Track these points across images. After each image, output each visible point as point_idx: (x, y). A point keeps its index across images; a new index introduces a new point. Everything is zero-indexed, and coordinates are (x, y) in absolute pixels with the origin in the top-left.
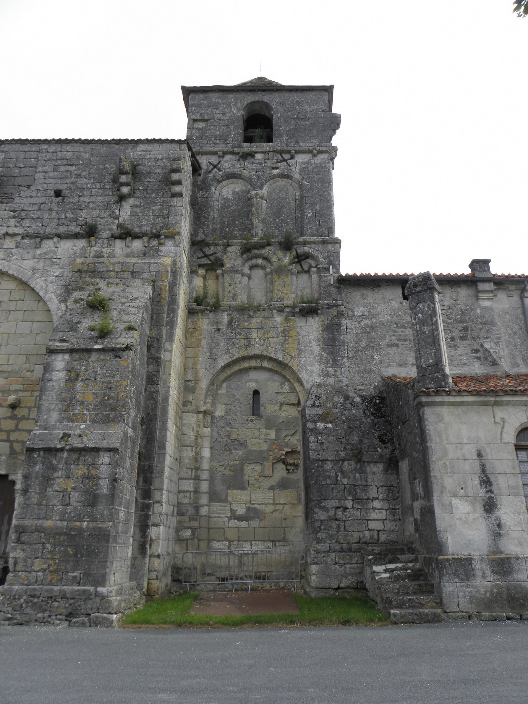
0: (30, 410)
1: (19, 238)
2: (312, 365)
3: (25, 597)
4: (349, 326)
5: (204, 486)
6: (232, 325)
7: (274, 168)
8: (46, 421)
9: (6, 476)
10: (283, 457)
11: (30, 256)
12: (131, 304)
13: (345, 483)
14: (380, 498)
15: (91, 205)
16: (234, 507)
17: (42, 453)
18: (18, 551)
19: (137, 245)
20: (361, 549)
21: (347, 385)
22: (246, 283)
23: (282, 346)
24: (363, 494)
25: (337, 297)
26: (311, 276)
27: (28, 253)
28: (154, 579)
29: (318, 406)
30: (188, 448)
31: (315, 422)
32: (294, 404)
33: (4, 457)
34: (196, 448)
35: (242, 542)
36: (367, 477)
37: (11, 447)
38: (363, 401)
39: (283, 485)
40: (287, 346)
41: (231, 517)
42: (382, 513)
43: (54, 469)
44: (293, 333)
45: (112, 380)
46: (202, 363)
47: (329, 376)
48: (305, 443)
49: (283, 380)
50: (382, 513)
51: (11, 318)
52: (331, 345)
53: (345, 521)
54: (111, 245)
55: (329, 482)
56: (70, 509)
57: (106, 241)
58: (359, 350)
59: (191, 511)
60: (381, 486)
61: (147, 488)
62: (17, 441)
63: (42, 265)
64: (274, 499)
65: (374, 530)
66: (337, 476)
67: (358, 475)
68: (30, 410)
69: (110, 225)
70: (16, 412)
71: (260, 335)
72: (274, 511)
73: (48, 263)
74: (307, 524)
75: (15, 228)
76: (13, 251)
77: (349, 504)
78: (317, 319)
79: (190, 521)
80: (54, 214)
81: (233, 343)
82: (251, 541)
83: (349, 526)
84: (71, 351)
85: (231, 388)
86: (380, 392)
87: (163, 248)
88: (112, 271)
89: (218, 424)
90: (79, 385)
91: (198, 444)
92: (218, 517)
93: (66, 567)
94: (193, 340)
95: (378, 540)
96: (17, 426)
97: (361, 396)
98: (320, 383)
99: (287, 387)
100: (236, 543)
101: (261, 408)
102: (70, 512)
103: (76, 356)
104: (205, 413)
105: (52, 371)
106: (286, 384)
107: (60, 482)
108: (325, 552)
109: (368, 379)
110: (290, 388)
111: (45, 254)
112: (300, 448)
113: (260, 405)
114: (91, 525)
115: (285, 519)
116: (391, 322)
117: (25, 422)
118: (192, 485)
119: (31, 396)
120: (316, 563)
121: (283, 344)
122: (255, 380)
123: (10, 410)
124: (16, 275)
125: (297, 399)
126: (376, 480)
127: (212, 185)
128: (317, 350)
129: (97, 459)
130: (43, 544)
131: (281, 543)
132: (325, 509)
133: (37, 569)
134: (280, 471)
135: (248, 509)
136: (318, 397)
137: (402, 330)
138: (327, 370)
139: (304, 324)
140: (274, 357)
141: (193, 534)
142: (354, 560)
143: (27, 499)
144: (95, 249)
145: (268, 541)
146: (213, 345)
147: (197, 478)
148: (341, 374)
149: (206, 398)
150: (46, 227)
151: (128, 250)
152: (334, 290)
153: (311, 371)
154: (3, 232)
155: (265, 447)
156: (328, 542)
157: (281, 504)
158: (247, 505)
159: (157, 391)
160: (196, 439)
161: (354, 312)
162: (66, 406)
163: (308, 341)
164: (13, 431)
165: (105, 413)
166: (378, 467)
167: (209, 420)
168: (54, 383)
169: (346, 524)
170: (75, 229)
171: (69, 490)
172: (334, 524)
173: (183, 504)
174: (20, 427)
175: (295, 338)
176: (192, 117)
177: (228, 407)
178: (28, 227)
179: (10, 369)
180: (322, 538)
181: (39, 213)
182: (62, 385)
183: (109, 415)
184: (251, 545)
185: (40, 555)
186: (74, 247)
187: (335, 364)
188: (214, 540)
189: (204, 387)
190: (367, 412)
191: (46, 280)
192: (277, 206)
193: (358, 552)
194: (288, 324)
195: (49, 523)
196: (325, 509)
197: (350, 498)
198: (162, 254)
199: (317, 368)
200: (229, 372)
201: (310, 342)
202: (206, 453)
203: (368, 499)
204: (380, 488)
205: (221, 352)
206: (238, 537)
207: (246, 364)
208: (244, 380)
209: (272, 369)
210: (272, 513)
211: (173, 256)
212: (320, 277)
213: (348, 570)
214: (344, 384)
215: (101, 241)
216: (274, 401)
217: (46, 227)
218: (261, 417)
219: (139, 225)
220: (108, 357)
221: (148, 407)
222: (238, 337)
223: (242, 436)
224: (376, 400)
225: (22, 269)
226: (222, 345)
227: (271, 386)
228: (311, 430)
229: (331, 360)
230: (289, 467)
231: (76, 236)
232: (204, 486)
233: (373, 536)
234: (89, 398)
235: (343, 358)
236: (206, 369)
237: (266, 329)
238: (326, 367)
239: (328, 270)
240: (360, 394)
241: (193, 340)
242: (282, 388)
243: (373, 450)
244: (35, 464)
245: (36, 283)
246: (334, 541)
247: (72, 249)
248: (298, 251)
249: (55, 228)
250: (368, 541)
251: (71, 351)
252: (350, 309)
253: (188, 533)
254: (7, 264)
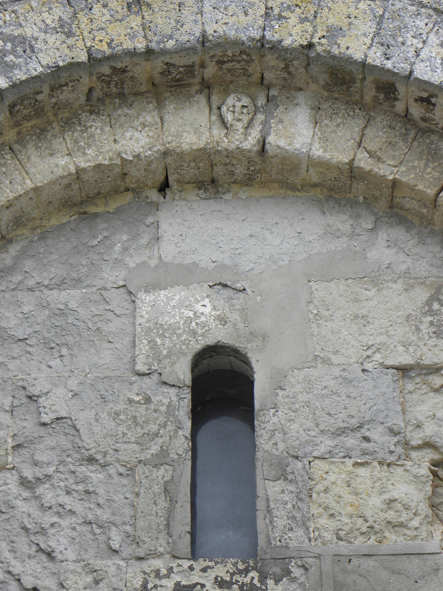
101: (271, 489)
113: (262, 470)
140: (375, 57)
208: (111, 276)
209: (353, 172)
216: (377, 434)
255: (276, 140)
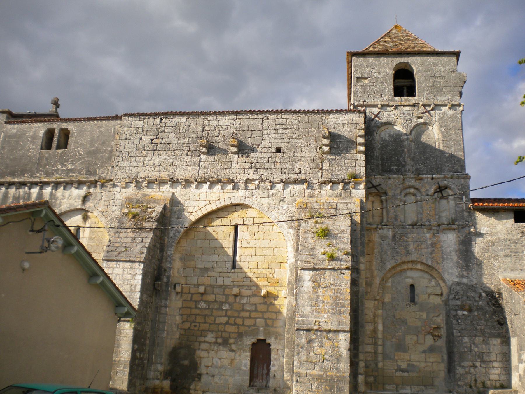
2: (452, 269)
5: (380, 349)
7: (419, 118)
10: (432, 331)
15: (303, 159)
16: (399, 363)
21: (476, 284)
26: (448, 202)
31: (456, 310)
32: (438, 295)
37: (265, 322)
38: (487, 295)
39: (432, 350)
40: (434, 255)
52: (465, 255)
55: (466, 350)
59: (373, 365)
64: (426, 359)
66: (471, 346)
67: (484, 346)
71: (415, 246)
80: (278, 166)
81: (397, 252)
90: (321, 290)
96: (268, 309)
99: (433, 283)
106: (433, 280)
110: (436, 284)
115: (433, 372)
116: (507, 239)
121: (431, 253)
127: (374, 131)
128: (455, 258)
132: (463, 367)
134: (429, 340)
136: (457, 293)
137: (514, 244)
141: (375, 380)
147: (375, 344)
148: (472, 276)
149: (379, 290)
153: (452, 273)
155: (419, 324)
164: (266, 312)
166: (497, 341)
175: (440, 249)
176: (356, 76)
179: (259, 272)
181: (268, 164)
189: (378, 282)
190: (490, 303)
191: (278, 213)
192: (422, 147)
196: (463, 367)
197: (479, 360)
199: (455, 271)
200: (394, 272)
201: (451, 253)
202: (380, 327)
230: (435, 338)
235: (473, 264)
238: (462, 271)
242: (430, 283)
244: (302, 338)
251: (314, 269)
253: (371, 379)
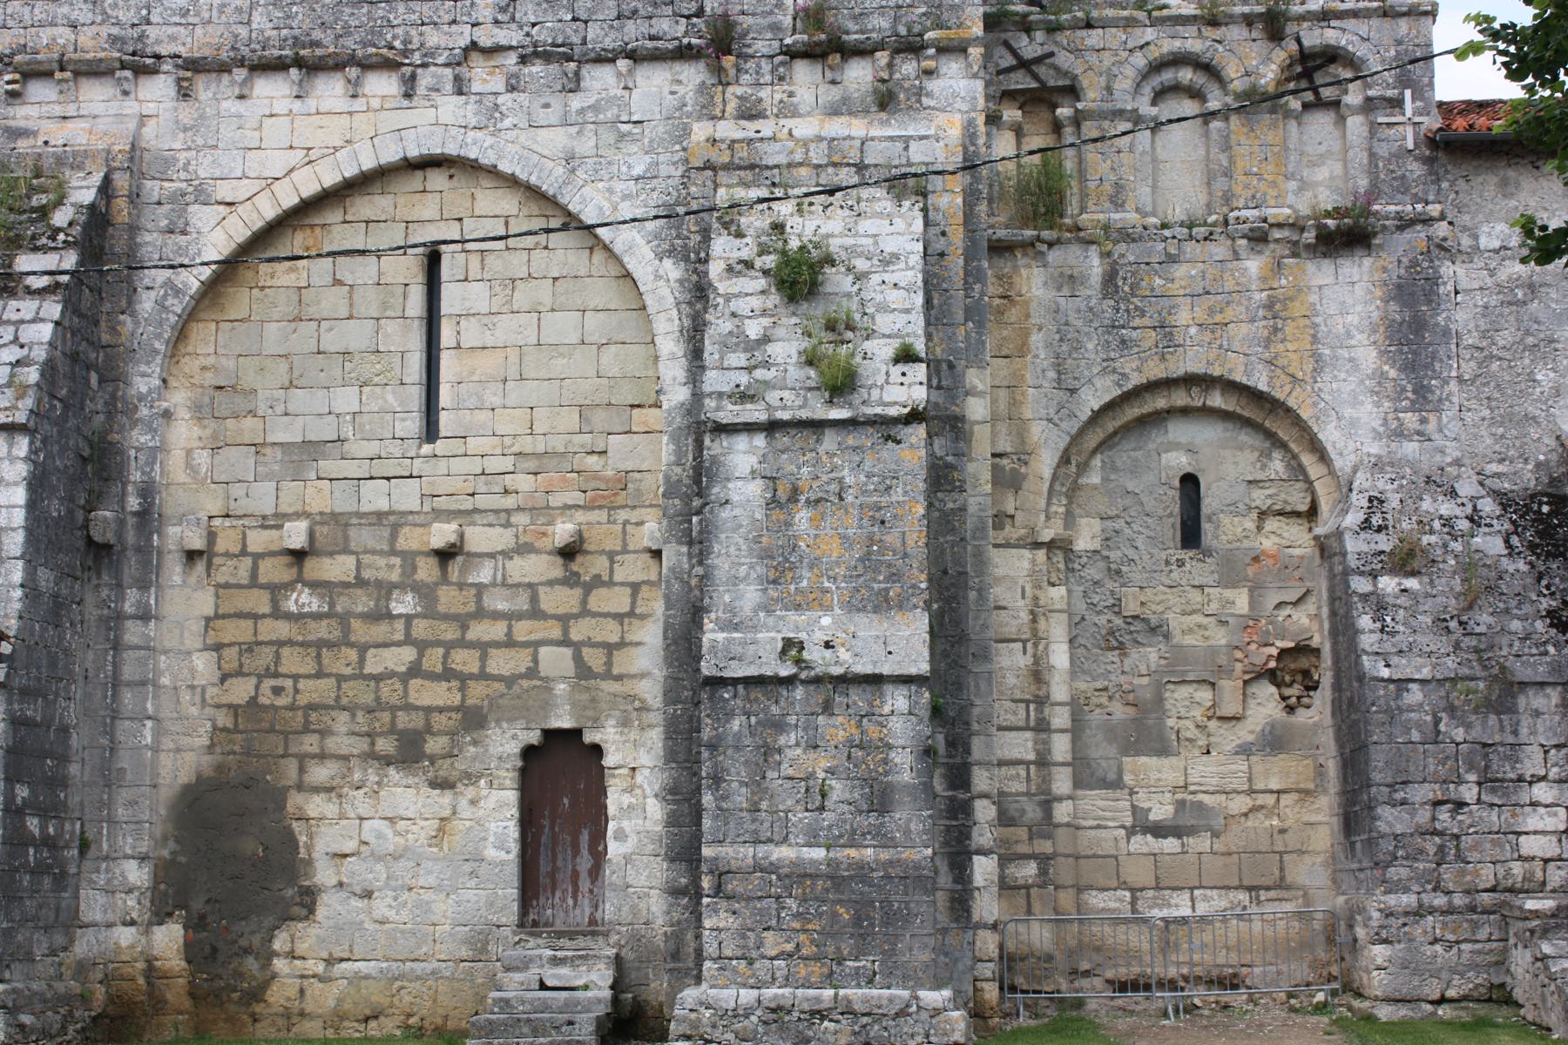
0: (612, 562)
1: (511, 59)
2: (1355, 403)
3: (759, 1012)
4: (1464, 284)
5: (1061, 747)
6: (1116, 286)
8: (731, 609)
9: (576, 733)
10: (1272, 664)
11: (553, 115)
12: (886, 277)
13: (1459, 739)
14: (1551, 775)
16: (1142, 800)
17: (740, 688)
18: (723, 915)
19: (859, 75)
20: (1504, 904)
21: (1457, 463)
22: (1148, 148)
23: (1266, 347)
24: (1508, 768)
25: (1426, 193)
27: (547, 106)
28: (987, 980)
29: (1379, 529)
30: (1012, 645)
31: (1374, 575)
32: (1297, 514)
33: (562, 686)
34: (1035, 645)
35: (1167, 892)
36: (1518, 723)
38: (1504, 507)
39: (1274, 742)
40: (1281, 347)
41: (1133, 827)
42: (1556, 814)
43: (779, 726)
44: (1297, 309)
45: (884, 500)
46: (1036, 403)
47: (1405, 437)
48: (1343, 629)
49: (1267, 444)
50: (1556, 814)
51: (522, 297)
53: (1457, 837)
54: (781, 79)
56: (828, 817)
57: (766, 66)
58: (1492, 357)
59: (1033, 812)
60: (1556, 746)
61: (958, 760)
62: (590, 643)
63: (592, 143)
64: (1250, 780)
65: (1533, 858)
66: (1437, 721)
68: (612, 562)
69: (771, 13)
70: (575, 567)
72: (1251, 811)
73: (609, 137)
74: (1352, 844)
75: (496, 31)
76: (500, 100)
77: (1469, 793)
78: (1367, 262)
79: (1031, 839)
81: (1123, 342)
82: (1192, 889)
83: (1470, 849)
84: (771, 427)
85: (1114, 469)
86: (1553, 481)
87: (932, 85)
88: (801, 164)
89: (1086, 573)
91: (1040, 634)
92: (1099, 827)
93: (838, 949)
94: (1005, 333)
95: (1544, 883)
97: (1497, 494)
98: (1379, 457)
99: (1277, 465)
100: (1151, 893)
102: (830, 827)
103: (783, 440)
104: (1051, 546)
105: (728, 480)
107: (794, 755)
108: (1407, 914)
109: (1518, 443)
110: (1288, 466)
111: (595, 108)
112: (1320, 639)
113: (1203, 519)
114: (885, 855)
117: (603, 591)
118: (1030, 744)
119: (609, 522)
120: (1386, 941)
121: (1268, 342)
122: (1184, 446)
123: (560, 560)
124: (523, 176)
125: (1309, 499)
126: (1541, 730)
128: (1369, 358)
129: (877, 702)
130: (778, 897)
131: (1272, 894)
133: (773, 953)
134: (1266, 705)
135: (1181, 804)
138: (1398, 419)
139: (1330, 280)
140: (1244, 381)
141: (1043, 872)
142: (1483, 934)
143: (724, 798)
144: (739, 91)
145: (1236, 888)
146: (1065, 348)
147: (1042, 727)
148: (1440, 431)
150: (586, 22)
151: (835, 93)
152: (1416, 169)
153: (1353, 423)
154: (464, 42)
156: (1416, 888)
157: (1272, 792)
158: (1179, 796)
159: (963, 509)
160: (1034, 621)
161: (1476, 237)
162: (776, 568)
163: (1342, 331)
164: (576, 617)
165: (876, 586)
166: (1548, 696)
167: (1062, 566)
168: (737, 512)
169: (1463, 845)
170: (671, 28)
171: (821, 775)
172: (1431, 845)
173: (1011, 794)
174: (593, 604)
177: (1109, 523)
178: (534, 25)
179: (541, 449)
180: (1400, 880)
182: (758, 516)
183: (887, 590)
184: (1192, 900)
185: (774, 922)
186: (675, 88)
187: (1422, 399)
188: (1091, 888)
189: (1047, 473)
190: (1515, 540)
191: (611, 191)
193: (1494, 913)
194: (1284, 282)
195: (783, 853)
197: (1472, 777)
198: (932, 103)
199: (1369, 413)
200: (1111, 425)
201: (1349, 335)
202: (1060, 657)
203: (1520, 779)
204: (1553, 751)
205: (1089, 366)
206: (1157, 878)
207: (1161, 403)
208: (1151, 446)
210: (1246, 815)
211: (965, 107)
212: (1374, 127)
213: (1465, 956)
214: (1449, 460)
215: (751, 65)
217: (586, 22)
218: (1208, 553)
219: (857, 11)
220: (866, 438)
221: (943, 552)
222: (1137, 322)
223: (1154, 607)
224: (1540, 504)
225: (535, 158)
226: (1090, 346)
227: (1230, 465)
228: (1365, 597)
229: (1409, 387)
231: (683, 53)
232: (1061, 747)
233: (1533, 874)
234: (832, 549)
235: (1446, 382)
236: (1050, 420)
237: (1219, 297)
239: (1397, 103)
240: (1496, 487)
241: (1005, 333)
242: (1264, 467)
243: (1534, 651)
244: (730, 715)
245: (583, 201)
246: (1429, 887)
247: (672, 93)
248: (1306, 43)
249: (611, 27)
250: (1518, 886)
252: (1465, 229)
253: (1030, 870)
254: (489, 141)
255: (1209, 403)
